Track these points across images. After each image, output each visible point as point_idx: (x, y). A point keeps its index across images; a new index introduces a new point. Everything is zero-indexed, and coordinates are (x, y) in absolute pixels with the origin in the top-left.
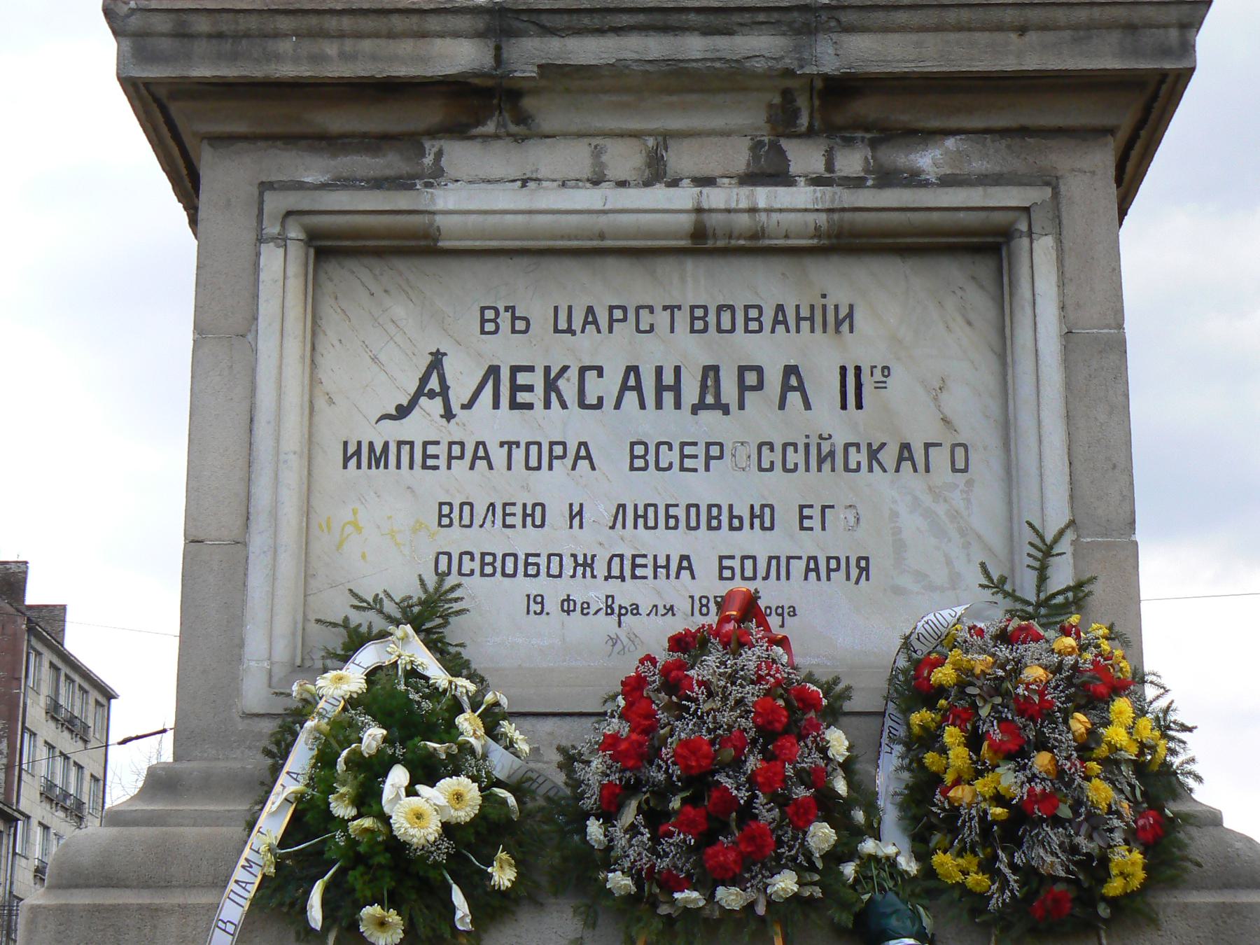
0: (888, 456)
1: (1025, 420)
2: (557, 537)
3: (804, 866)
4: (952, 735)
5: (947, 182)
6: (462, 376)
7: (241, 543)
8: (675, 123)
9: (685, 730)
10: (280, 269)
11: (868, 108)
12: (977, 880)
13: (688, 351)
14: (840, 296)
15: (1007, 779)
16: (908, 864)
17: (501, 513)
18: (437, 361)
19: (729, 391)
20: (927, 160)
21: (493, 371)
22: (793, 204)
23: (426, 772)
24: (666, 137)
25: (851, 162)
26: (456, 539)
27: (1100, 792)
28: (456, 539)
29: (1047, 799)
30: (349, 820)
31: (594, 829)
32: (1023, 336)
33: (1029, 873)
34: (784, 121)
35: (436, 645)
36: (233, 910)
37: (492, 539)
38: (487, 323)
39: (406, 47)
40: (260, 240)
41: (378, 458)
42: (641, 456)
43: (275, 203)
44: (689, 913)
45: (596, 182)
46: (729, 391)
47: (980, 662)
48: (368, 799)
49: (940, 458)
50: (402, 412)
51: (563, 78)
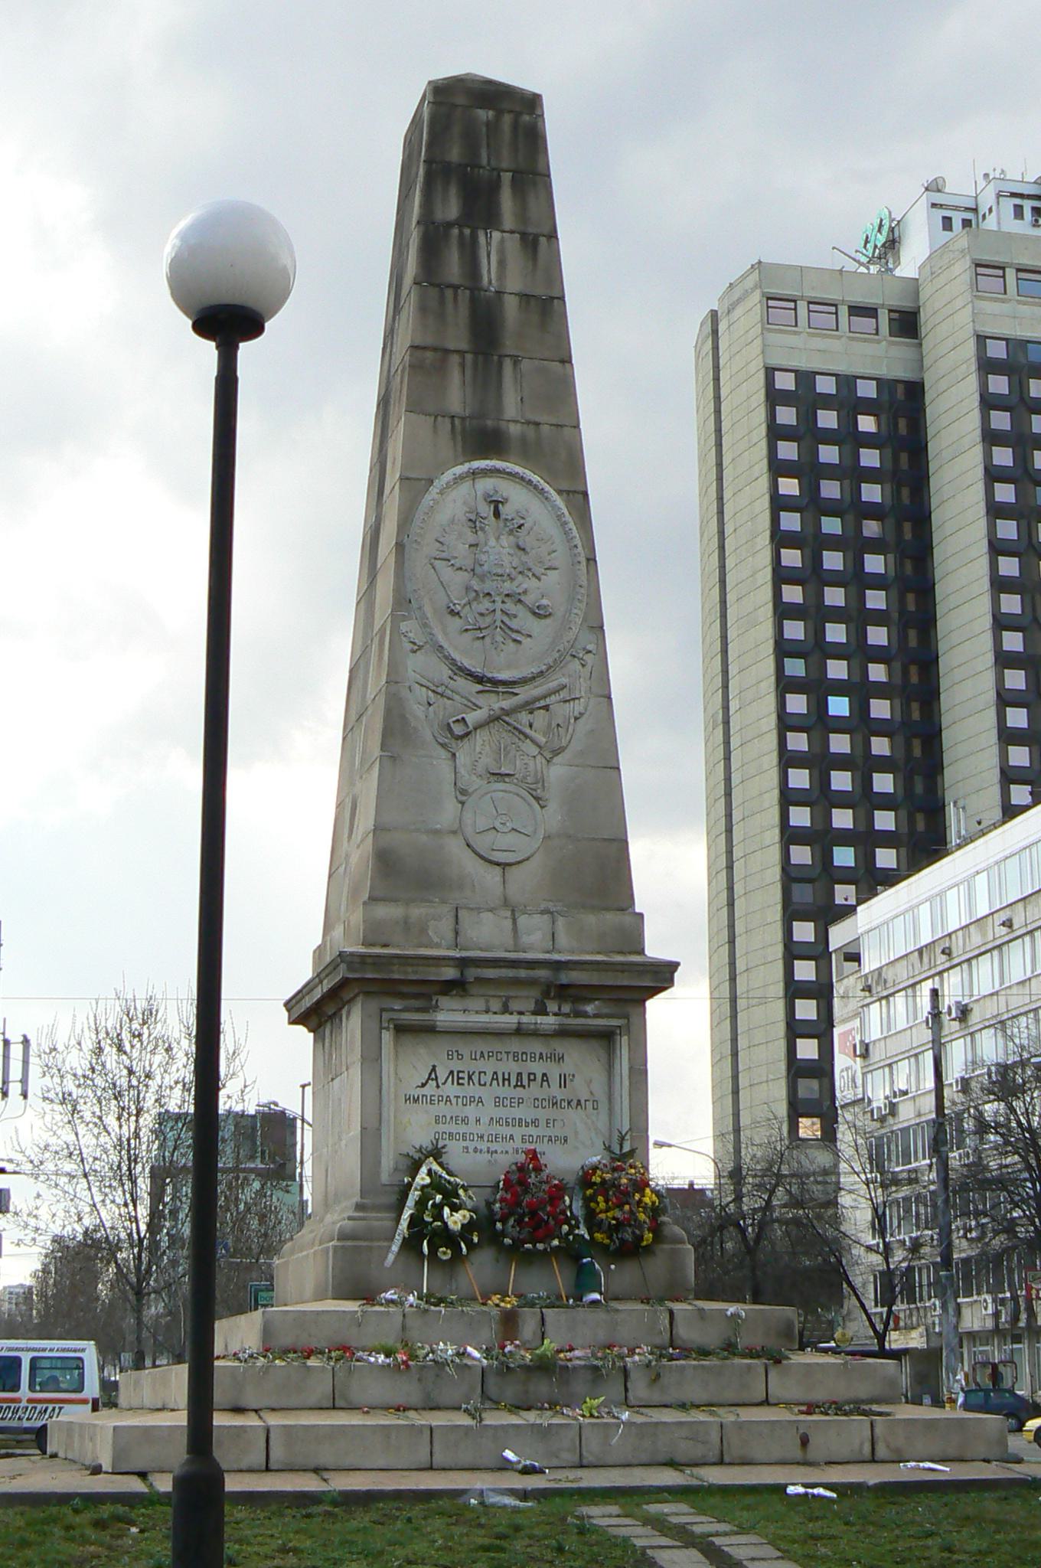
0: (574, 1104)
1: (617, 1095)
2: (472, 1128)
3: (560, 1238)
4: (600, 1199)
5: (596, 1016)
6: (442, 1075)
7: (379, 1129)
8: (511, 994)
9: (527, 1198)
10: (387, 1037)
11: (572, 991)
12: (607, 1241)
13: (511, 1067)
14: (560, 1050)
15: (617, 1213)
16: (587, 1236)
17: (454, 1119)
18: (434, 1067)
19: (525, 1082)
20: (590, 1008)
21: (452, 1072)
22: (548, 1022)
23: (454, 1208)
24: (508, 998)
25: (566, 1008)
26: (441, 1128)
27: (642, 1217)
28: (441, 1128)
29: (628, 1220)
30: (997, 1325)
31: (499, 1225)
32: (617, 1066)
33: (622, 1241)
34: (546, 994)
35: (441, 1164)
36: (395, 1248)
37: (453, 1128)
38: (450, 1056)
39: (433, 969)
40: (381, 1028)
41: (416, 1100)
42: (498, 1102)
43: (385, 1015)
44: (528, 1250)
45: (487, 1012)
46: (525, 1082)
47: (608, 1176)
48: (439, 1216)
49: (589, 1105)
50: (423, 1085)
51: (480, 981)
